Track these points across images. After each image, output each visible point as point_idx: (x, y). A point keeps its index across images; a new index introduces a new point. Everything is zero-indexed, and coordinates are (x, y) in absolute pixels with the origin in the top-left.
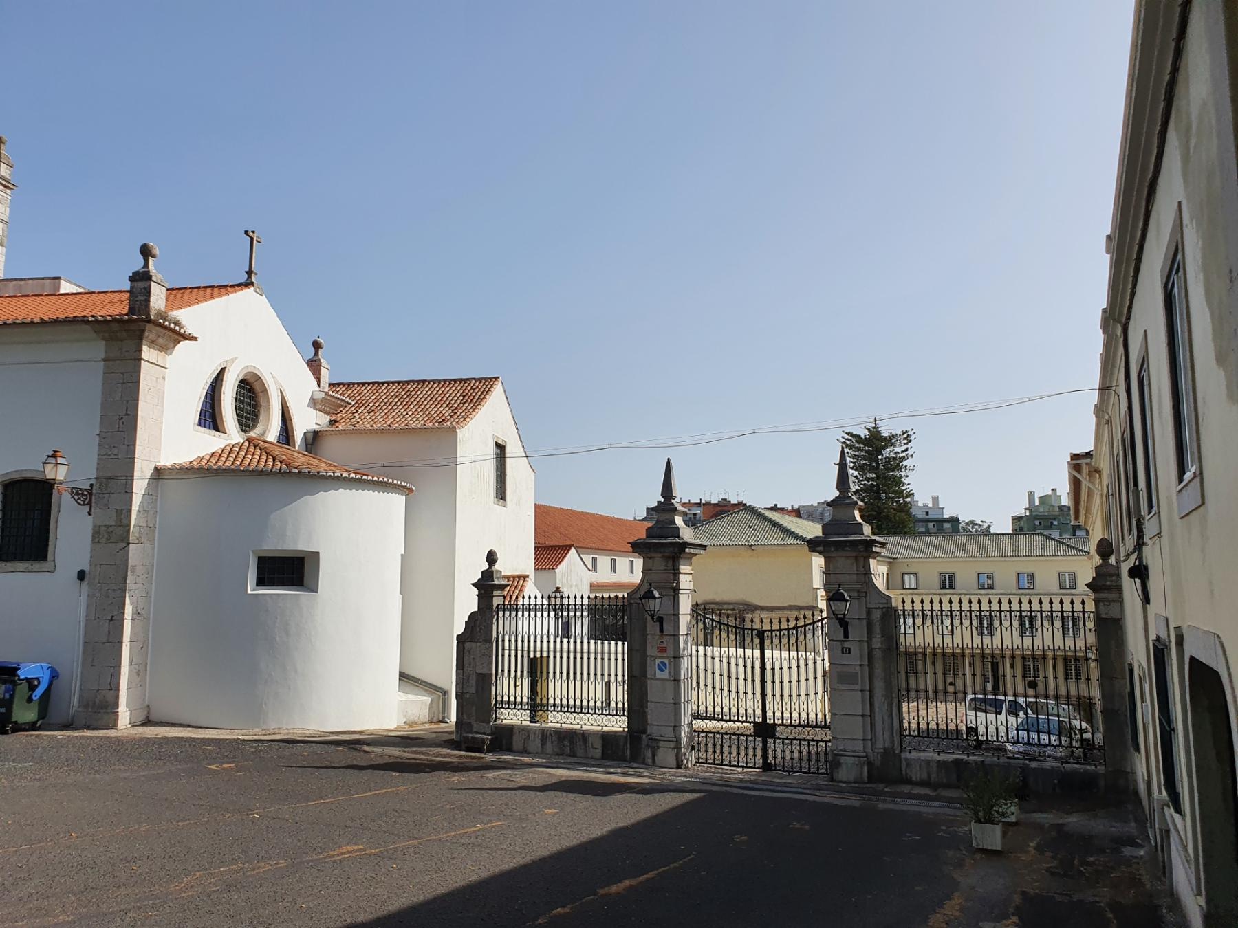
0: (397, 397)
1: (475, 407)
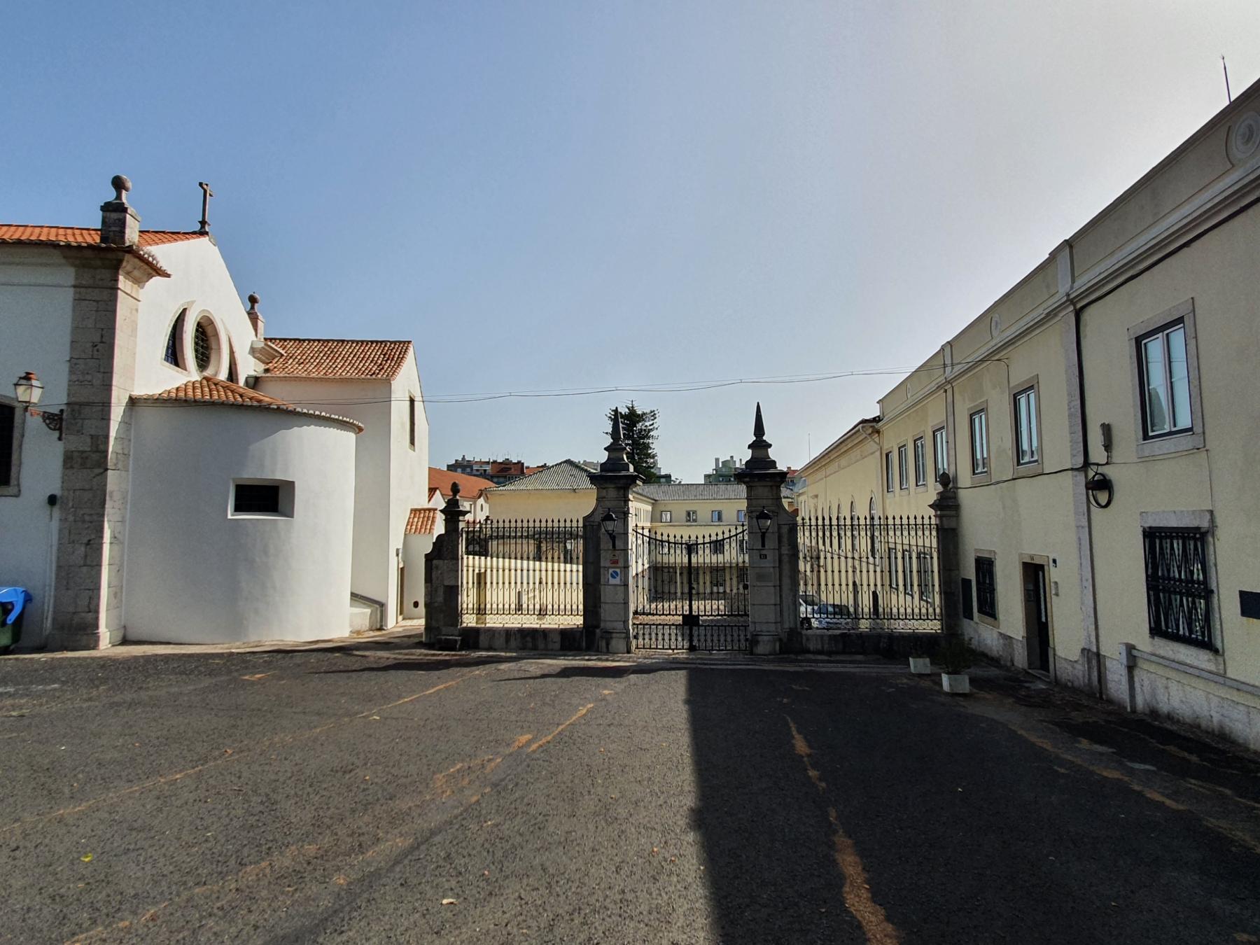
0: (321, 352)
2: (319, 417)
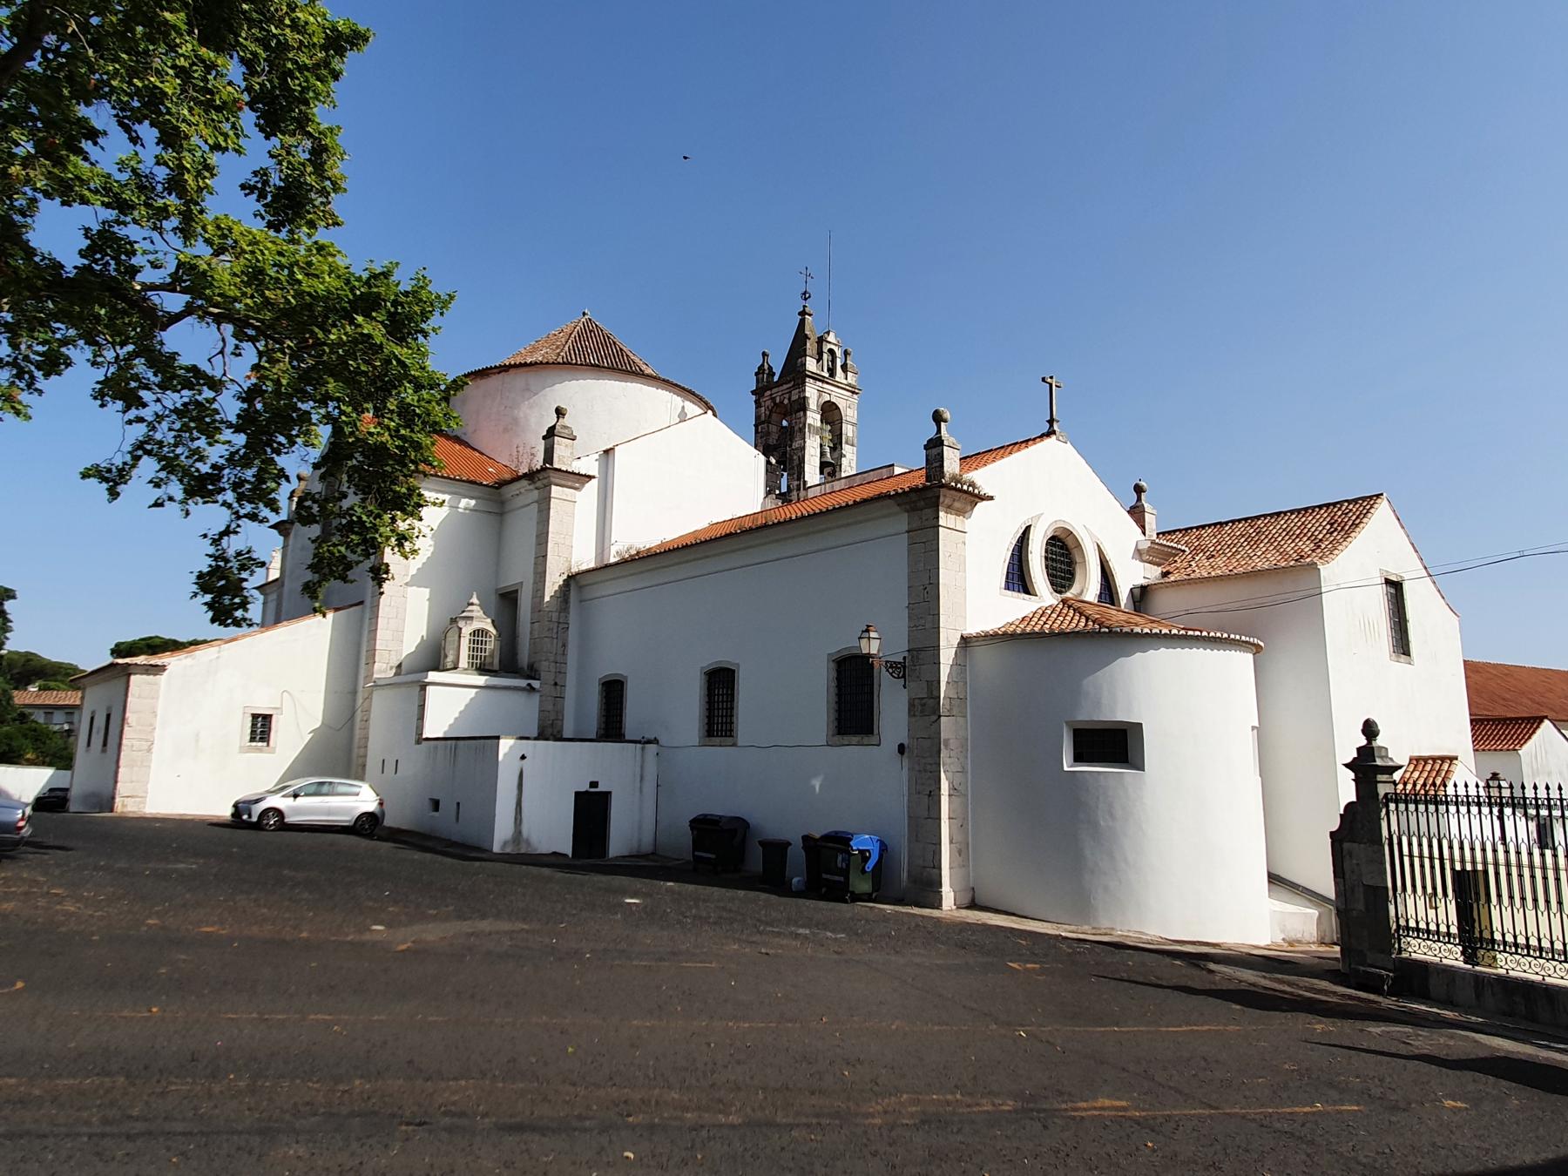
1: (1348, 535)
2: (1158, 636)
